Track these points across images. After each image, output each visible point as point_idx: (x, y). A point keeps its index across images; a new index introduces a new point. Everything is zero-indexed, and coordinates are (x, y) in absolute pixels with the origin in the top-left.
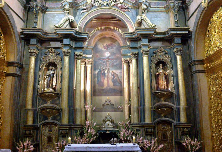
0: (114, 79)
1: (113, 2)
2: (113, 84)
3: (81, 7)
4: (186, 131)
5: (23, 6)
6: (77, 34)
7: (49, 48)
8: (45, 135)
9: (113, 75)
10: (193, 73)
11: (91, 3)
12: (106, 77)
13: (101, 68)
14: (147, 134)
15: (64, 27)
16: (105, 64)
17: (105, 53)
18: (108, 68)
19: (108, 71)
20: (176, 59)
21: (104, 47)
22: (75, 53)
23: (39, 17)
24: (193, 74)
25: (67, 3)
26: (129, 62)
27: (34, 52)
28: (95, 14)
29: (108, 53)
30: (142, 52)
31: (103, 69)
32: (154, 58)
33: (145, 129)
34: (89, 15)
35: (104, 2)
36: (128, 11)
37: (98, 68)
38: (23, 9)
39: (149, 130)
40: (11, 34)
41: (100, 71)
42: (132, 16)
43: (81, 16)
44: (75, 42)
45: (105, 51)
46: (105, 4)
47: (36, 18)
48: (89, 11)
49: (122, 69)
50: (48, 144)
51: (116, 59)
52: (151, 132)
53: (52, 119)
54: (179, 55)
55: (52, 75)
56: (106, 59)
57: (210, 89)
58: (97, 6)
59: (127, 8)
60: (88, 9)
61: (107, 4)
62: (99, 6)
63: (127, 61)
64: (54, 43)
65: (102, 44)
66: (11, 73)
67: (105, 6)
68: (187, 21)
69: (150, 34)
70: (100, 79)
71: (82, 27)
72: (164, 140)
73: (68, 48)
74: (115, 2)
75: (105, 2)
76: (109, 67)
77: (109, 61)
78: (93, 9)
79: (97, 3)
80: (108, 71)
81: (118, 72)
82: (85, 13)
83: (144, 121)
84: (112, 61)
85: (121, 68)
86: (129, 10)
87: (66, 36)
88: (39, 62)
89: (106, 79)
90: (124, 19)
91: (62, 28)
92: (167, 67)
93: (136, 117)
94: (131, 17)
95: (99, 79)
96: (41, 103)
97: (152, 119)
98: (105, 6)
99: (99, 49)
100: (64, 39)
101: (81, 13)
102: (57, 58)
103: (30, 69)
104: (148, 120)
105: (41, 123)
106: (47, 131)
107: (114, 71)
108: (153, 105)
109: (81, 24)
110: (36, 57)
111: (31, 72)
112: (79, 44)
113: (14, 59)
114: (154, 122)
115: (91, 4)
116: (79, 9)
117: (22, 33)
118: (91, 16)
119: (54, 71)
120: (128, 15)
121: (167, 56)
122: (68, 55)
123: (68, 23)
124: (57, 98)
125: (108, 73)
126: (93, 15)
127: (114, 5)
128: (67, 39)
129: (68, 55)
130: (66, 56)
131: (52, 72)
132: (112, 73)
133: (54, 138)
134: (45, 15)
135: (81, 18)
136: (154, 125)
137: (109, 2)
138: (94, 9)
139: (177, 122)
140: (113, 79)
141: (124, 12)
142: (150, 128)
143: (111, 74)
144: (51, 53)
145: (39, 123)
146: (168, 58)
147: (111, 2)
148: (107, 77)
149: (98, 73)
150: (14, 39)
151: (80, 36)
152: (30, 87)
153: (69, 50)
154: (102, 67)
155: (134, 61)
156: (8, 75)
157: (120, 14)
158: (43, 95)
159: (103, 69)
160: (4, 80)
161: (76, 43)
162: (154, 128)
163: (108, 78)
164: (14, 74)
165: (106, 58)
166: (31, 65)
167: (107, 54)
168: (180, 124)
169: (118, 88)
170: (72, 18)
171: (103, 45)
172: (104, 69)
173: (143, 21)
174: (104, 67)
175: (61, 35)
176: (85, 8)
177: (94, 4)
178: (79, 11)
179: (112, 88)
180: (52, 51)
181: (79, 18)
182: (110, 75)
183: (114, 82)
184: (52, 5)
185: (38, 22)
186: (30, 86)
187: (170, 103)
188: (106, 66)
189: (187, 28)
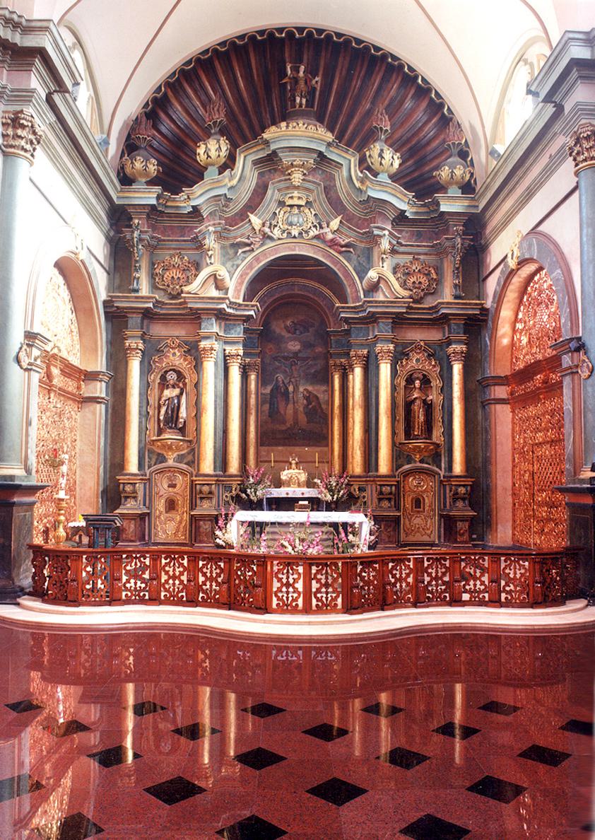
0: (310, 406)
1: (314, 229)
4: (462, 492)
5: (107, 213)
6: (231, 308)
8: (161, 494)
9: (307, 398)
10: (487, 403)
13: (280, 379)
14: (381, 496)
16: (287, 369)
18: (296, 381)
20: (450, 368)
21: (286, 327)
22: (225, 350)
24: (485, 404)
26: (345, 369)
27: (137, 349)
29: (297, 343)
30: (379, 353)
31: (283, 383)
32: (403, 366)
33: (378, 487)
35: (294, 227)
39: (386, 489)
42: (357, 264)
46: (295, 232)
49: (328, 383)
50: (168, 515)
52: (391, 493)
53: (176, 462)
54: (457, 362)
57: (495, 657)
61: (300, 234)
62: (281, 237)
65: (282, 321)
67: (295, 237)
68: (481, 282)
72: (418, 512)
73: (91, 511)
74: (318, 228)
75: (295, 227)
76: (298, 379)
79: (277, 229)
81: (318, 390)
83: (377, 470)
85: (328, 381)
86: (352, 250)
89: (290, 406)
90: (337, 271)
92: (431, 387)
93: (359, 461)
94: (355, 266)
95: (274, 407)
96: (154, 460)
97: (393, 467)
98: (295, 237)
99: (275, 332)
102: (185, 360)
104: (384, 468)
105: (153, 469)
106: (166, 486)
107: (310, 388)
108: (397, 470)
110: (142, 359)
114: (397, 474)
120: (349, 260)
121: (433, 363)
132: (305, 393)
133: (180, 502)
135: (238, 266)
136: (397, 479)
139: (447, 474)
142: (388, 485)
145: (149, 468)
146: (434, 366)
147: (309, 227)
148: (294, 403)
155: (358, 371)
159: (283, 383)
162: (398, 487)
163: (296, 404)
167: (294, 346)
168: (452, 477)
172: (286, 382)
173: (382, 282)
174: (285, 378)
181: (233, 265)
187: (433, 465)
188: (291, 376)
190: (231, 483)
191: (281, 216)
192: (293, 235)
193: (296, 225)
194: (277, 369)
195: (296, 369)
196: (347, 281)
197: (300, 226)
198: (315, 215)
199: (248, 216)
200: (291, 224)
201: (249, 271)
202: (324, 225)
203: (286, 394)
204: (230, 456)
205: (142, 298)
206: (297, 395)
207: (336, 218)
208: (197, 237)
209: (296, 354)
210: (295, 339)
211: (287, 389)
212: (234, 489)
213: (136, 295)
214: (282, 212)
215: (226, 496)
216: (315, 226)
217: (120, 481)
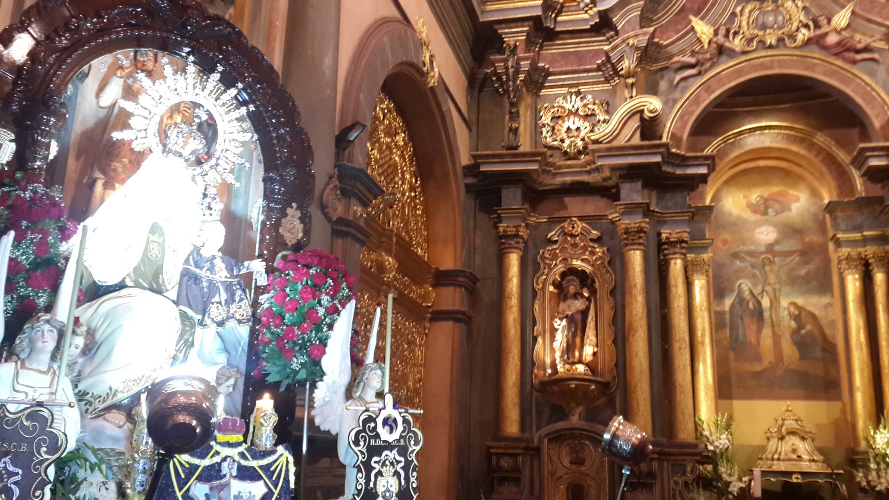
0: (803, 332)
1: (804, 31)
2: (797, 354)
3: (676, 59)
7: (563, 219)
8: (558, 474)
9: (797, 318)
11: (715, 40)
12: (767, 324)
15: (621, 141)
16: (757, 272)
17: (758, 230)
18: (775, 290)
19: (775, 302)
22: (659, 234)
23: (522, 110)
25: (627, 49)
28: (729, 82)
29: (771, 228)
31: (752, 293)
34: (709, 87)
36: (872, 60)
37: (732, 291)
38: (466, 83)
40: (446, 175)
41: (740, 300)
43: (677, 94)
44: (657, 192)
45: (756, 221)
46: (771, 40)
47: (515, 116)
48: (706, 71)
51: (803, 253)
55: (579, 317)
56: (762, 253)
58: (737, 49)
59: (867, 49)
60: (702, 64)
61: (780, 40)
63: (862, 258)
64: (578, 199)
66: (450, 308)
69: (527, 173)
70: (740, 331)
71: (683, 133)
73: (641, 216)
75: (771, 31)
76: (777, 286)
77: (777, 259)
78: (725, 62)
80: (774, 299)
81: (814, 303)
82: (691, 80)
84: (789, 259)
87: (631, 173)
88: (530, 270)
89: (767, 332)
90: (852, 94)
91: (615, 143)
95: (738, 334)
98: (771, 47)
100: (624, 185)
101: (678, 83)
103: (507, 295)
105: (544, 431)
106: (566, 461)
107: (800, 301)
109: (679, 125)
111: (512, 307)
112: (675, 199)
113: (455, 262)
115: (714, 45)
116: (666, 68)
117: (472, 170)
118: (713, 91)
119: (588, 299)
120: (872, 74)
122: (641, 241)
123: (635, 123)
124: (602, 400)
125: (776, 309)
126: (724, 85)
127: (809, 40)
128: (632, 182)
129: (641, 241)
130: (635, 247)
131: (579, 304)
132: (792, 309)
134: (538, 100)
135: (675, 101)
137: (785, 30)
138: (725, 65)
140: (795, 332)
141: (854, 62)
143: (786, 313)
144: (572, 236)
145: (537, 430)
148: (773, 326)
149: (732, 307)
150: (454, 193)
151: (679, 172)
152: (511, 359)
153: (643, 225)
154: (745, 285)
156: (439, 316)
157: (834, 72)
158: (555, 388)
159: (752, 293)
160: (426, 335)
161: (660, 198)
163: (776, 329)
164: (458, 312)
165: (763, 249)
166: (510, 280)
169: (816, 369)
170: (653, 104)
171: (745, 197)
175: (613, 168)
176: (693, 60)
177: (727, 44)
178: (668, 75)
179: (792, 367)
180: (573, 227)
182: (781, 314)
183: (803, 344)
184: (563, 62)
185: (521, 129)
186: (512, 355)
188: (766, 281)
189: (479, 153)
190: (683, 458)
191: (745, 18)
192: (768, 43)
193: (772, 27)
194: (739, 274)
195: (771, 271)
196: (872, 109)
197: (780, 28)
198: (804, 8)
199: (690, 21)
200: (764, 27)
201: (694, 108)
202: (823, 20)
203: (759, 314)
204: (678, 411)
205: (524, 155)
206: (777, 313)
207: (843, 7)
208: (608, 58)
209: (770, 248)
210: (767, 223)
211: (759, 303)
212: (689, 469)
213: (516, 151)
214: (747, 11)
215: (676, 483)
216: (807, 26)
217: (492, 451)
